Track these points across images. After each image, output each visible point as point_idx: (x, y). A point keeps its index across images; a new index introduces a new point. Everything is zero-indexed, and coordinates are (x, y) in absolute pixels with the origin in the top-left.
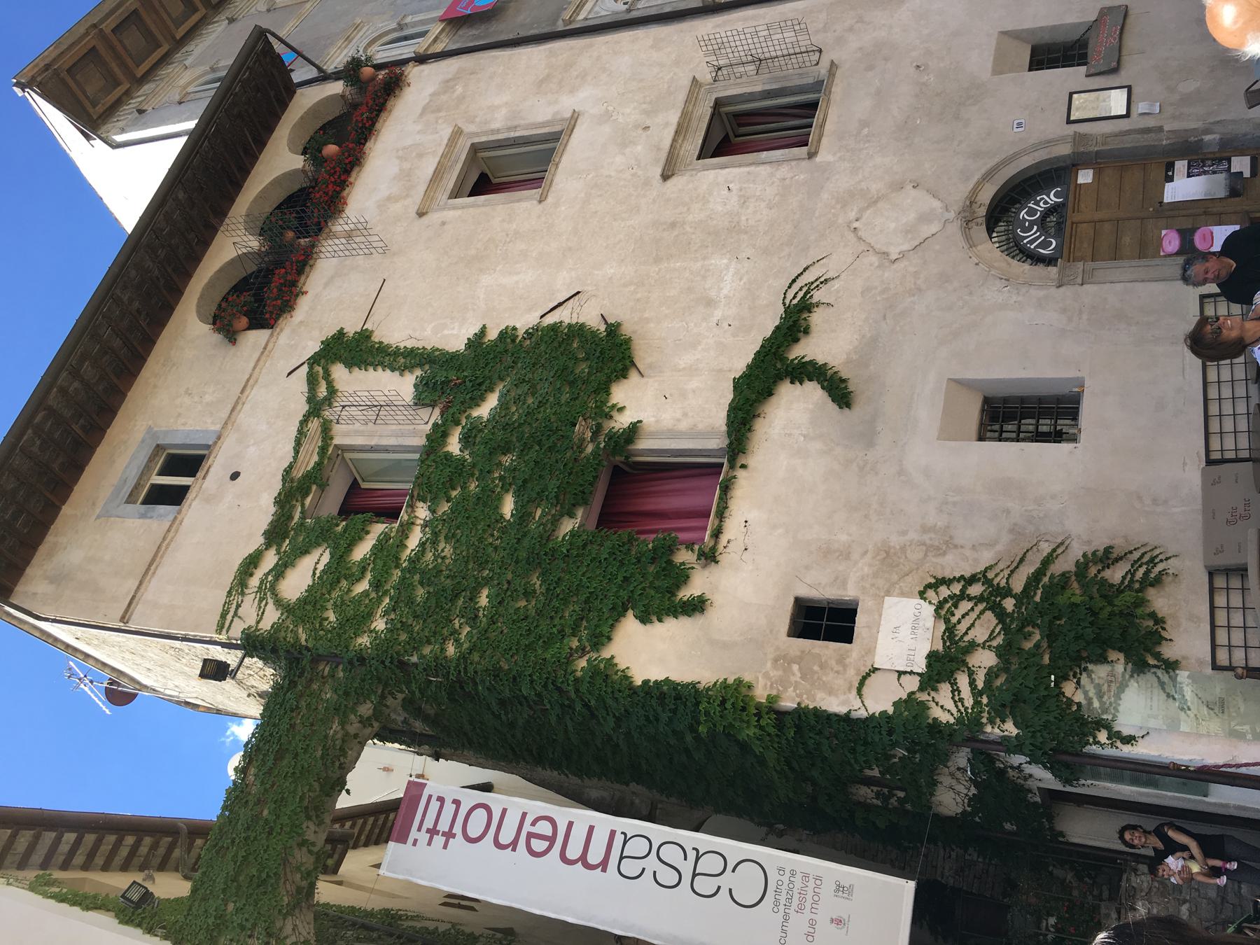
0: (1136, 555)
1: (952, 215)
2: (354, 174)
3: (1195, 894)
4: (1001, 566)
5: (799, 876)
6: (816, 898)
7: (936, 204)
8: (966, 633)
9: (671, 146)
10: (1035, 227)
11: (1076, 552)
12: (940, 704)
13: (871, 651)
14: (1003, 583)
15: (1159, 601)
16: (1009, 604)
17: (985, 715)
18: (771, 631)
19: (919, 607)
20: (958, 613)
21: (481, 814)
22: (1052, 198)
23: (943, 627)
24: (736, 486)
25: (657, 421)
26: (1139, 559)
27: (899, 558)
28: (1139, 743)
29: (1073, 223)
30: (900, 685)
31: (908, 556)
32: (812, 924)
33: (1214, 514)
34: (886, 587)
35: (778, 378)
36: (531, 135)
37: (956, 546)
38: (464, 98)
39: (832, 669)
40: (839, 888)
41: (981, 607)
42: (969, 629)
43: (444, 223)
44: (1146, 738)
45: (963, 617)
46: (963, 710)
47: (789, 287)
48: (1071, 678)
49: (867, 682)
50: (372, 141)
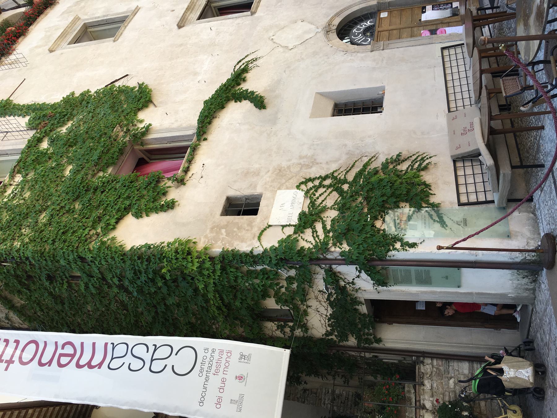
0: (414, 157)
1: (320, 30)
2: (20, 39)
3: (457, 373)
4: (341, 170)
6: (227, 364)
7: (313, 27)
8: (322, 203)
9: (184, 14)
10: (360, 35)
11: (382, 159)
12: (305, 239)
13: (267, 217)
14: (342, 177)
15: (427, 177)
16: (346, 187)
17: (331, 242)
18: (211, 215)
19: (296, 193)
20: (317, 194)
21: (33, 346)
22: (369, 23)
23: (308, 201)
24: (200, 149)
25: (161, 125)
26: (415, 159)
27: (286, 171)
28: (419, 247)
29: (378, 32)
30: (283, 232)
31: (291, 170)
32: (223, 381)
33: (454, 132)
34: (278, 186)
35: (228, 100)
36: (115, 18)
37: (317, 164)
38: (84, 7)
39: (244, 229)
41: (330, 190)
42: (323, 201)
43: (62, 54)
44: (423, 244)
45: (320, 195)
46: (318, 241)
47: (237, 64)
48: (380, 218)
49: (264, 233)
50: (34, 26)
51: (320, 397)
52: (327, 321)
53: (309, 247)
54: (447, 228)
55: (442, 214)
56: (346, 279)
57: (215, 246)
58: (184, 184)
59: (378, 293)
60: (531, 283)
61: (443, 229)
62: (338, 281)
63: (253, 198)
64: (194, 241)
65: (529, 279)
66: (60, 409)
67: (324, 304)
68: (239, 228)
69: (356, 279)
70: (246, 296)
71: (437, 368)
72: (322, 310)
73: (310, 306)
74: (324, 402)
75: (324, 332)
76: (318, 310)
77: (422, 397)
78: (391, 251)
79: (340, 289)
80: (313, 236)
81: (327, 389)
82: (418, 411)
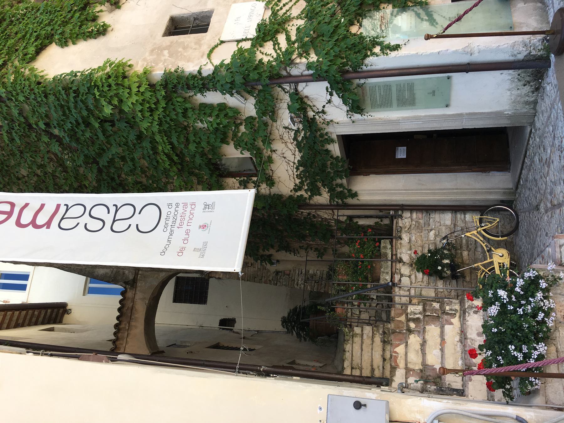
5: (181, 206)
6: (191, 216)
12: (265, 53)
13: (219, 33)
18: (151, 36)
23: (269, 13)
32: (187, 233)
40: (206, 206)
45: (284, 5)
49: (215, 51)
51: (293, 278)
52: (295, 170)
53: (269, 60)
54: (437, 26)
55: (432, 11)
56: (314, 106)
57: (155, 68)
58: (119, 8)
59: (353, 122)
60: (533, 92)
61: (433, 27)
62: (305, 112)
63: (203, 17)
64: (129, 63)
65: (531, 86)
66: (27, 314)
67: (290, 145)
68: (185, 48)
69: (327, 105)
70: (200, 138)
71: (416, 222)
72: (289, 155)
73: (274, 151)
74: (297, 282)
75: (292, 186)
76: (285, 155)
77: (398, 251)
78: (369, 56)
79: (308, 121)
80: (274, 49)
81: (300, 270)
82: (394, 264)
